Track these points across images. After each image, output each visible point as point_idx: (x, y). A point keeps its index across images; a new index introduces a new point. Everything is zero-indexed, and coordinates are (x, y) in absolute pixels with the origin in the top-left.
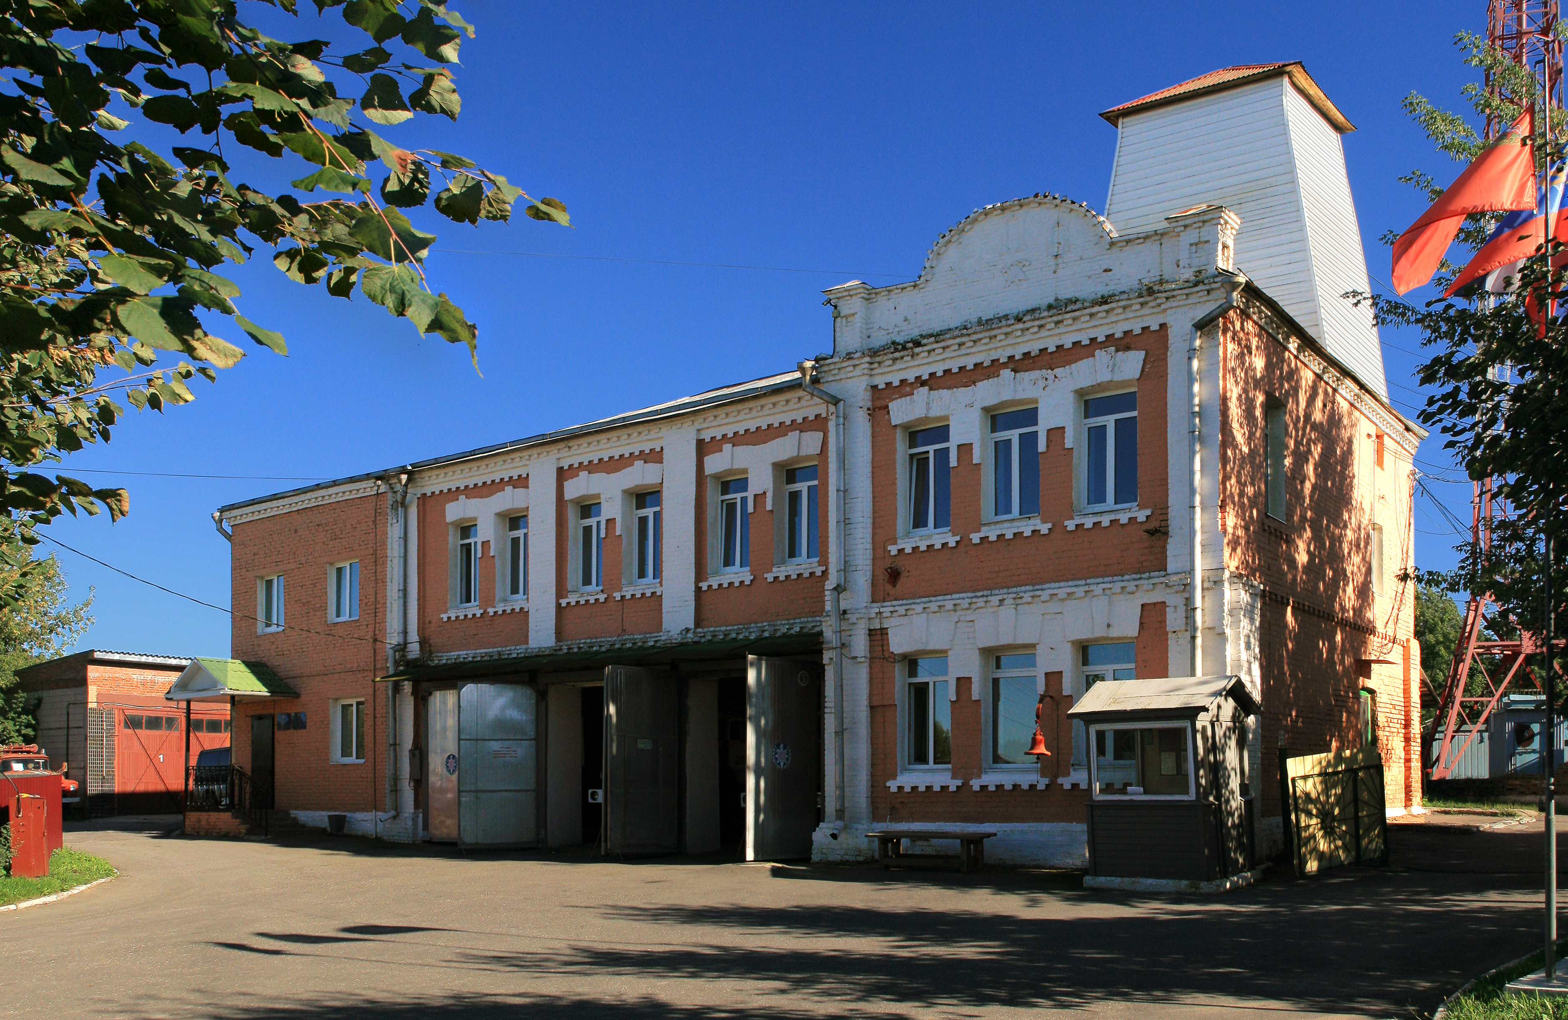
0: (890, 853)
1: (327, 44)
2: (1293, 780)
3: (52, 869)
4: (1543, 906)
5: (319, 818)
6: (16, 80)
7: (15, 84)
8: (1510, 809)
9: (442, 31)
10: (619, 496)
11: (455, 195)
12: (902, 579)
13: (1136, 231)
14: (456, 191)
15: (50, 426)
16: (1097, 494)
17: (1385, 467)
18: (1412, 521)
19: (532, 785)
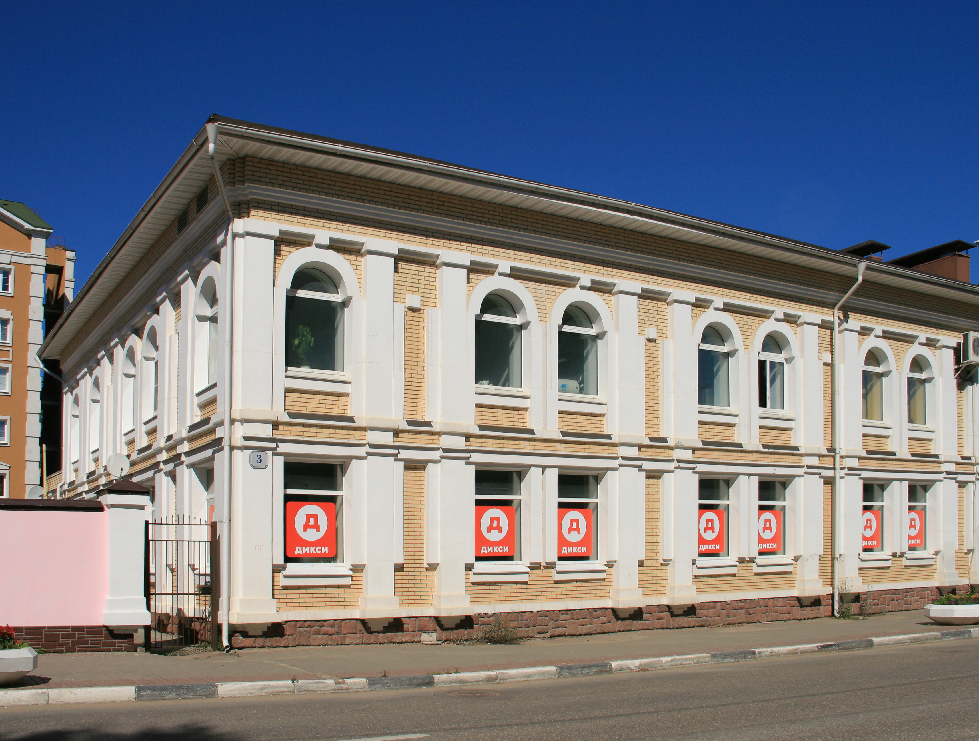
0: (835, 613)
1: (51, 679)
2: (693, 457)
3: (285, 633)
4: (277, 257)
5: (480, 683)
6: (157, 349)
7: (43, 675)
8: (729, 664)
9: (231, 224)
10: (478, 385)
11: (52, 242)
12: (694, 558)
13: (216, 200)
14: (38, 245)
15: (807, 560)
16: (78, 634)
17: (50, 677)
18: (527, 670)
19: (210, 539)
